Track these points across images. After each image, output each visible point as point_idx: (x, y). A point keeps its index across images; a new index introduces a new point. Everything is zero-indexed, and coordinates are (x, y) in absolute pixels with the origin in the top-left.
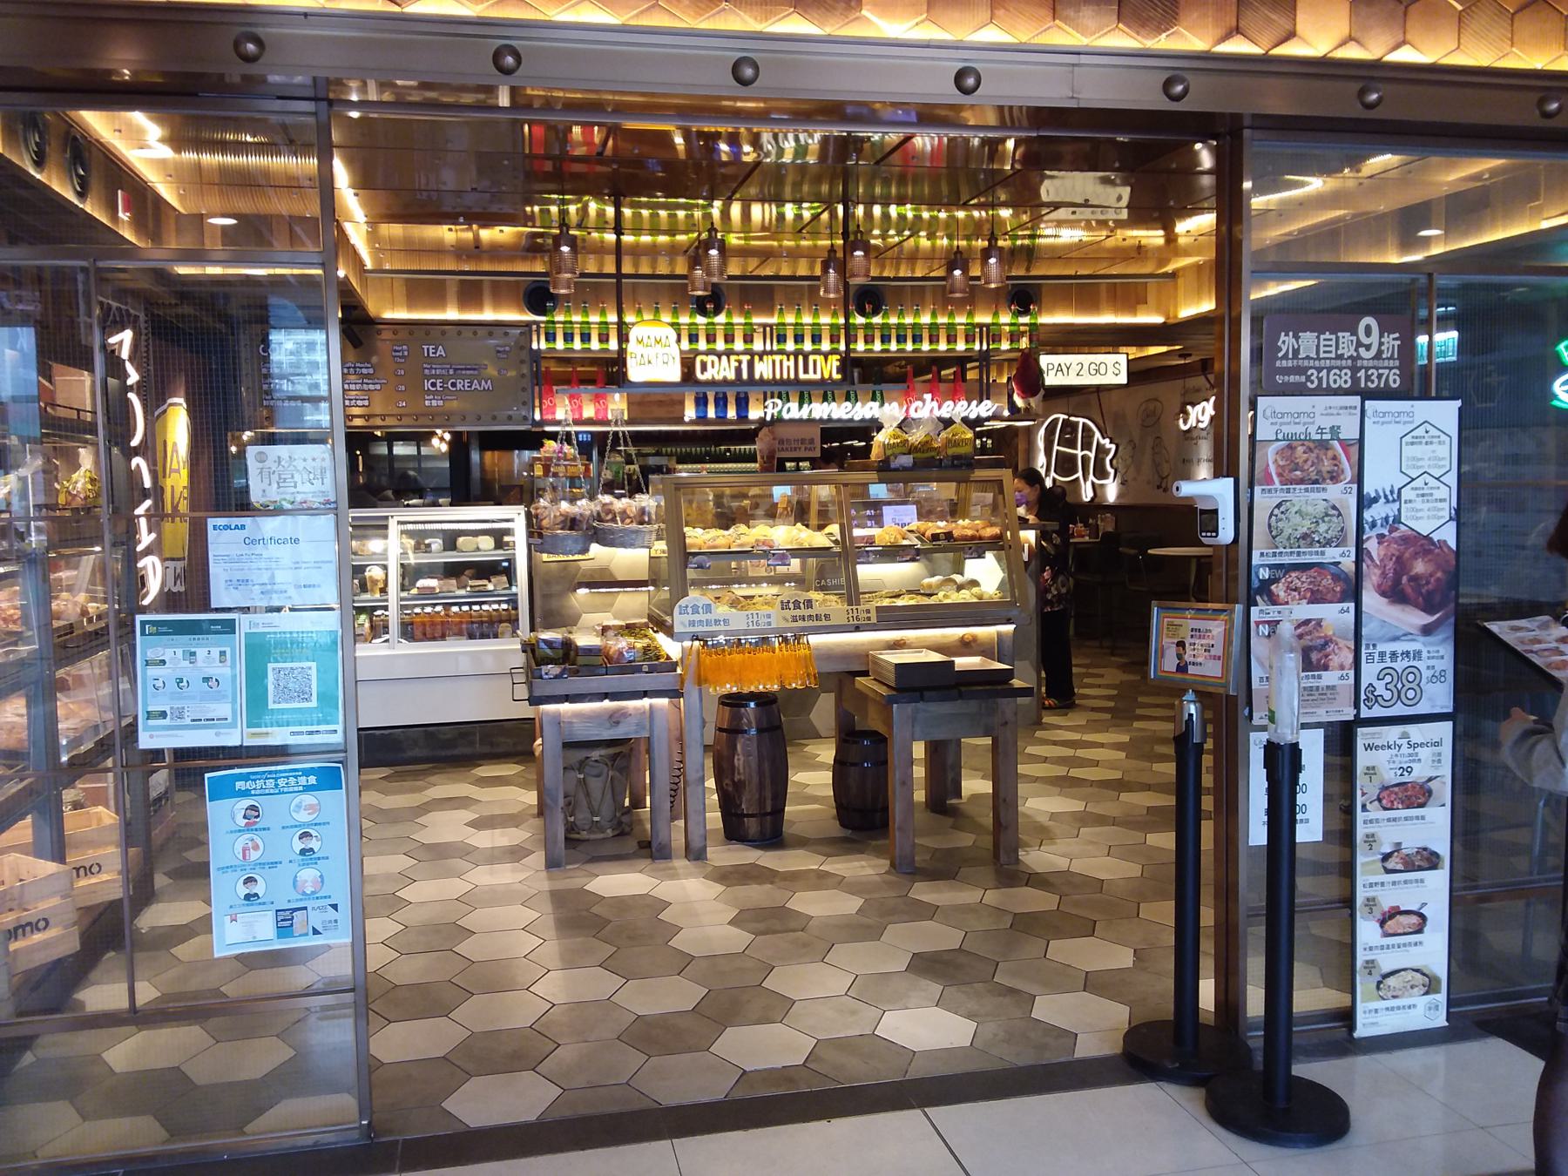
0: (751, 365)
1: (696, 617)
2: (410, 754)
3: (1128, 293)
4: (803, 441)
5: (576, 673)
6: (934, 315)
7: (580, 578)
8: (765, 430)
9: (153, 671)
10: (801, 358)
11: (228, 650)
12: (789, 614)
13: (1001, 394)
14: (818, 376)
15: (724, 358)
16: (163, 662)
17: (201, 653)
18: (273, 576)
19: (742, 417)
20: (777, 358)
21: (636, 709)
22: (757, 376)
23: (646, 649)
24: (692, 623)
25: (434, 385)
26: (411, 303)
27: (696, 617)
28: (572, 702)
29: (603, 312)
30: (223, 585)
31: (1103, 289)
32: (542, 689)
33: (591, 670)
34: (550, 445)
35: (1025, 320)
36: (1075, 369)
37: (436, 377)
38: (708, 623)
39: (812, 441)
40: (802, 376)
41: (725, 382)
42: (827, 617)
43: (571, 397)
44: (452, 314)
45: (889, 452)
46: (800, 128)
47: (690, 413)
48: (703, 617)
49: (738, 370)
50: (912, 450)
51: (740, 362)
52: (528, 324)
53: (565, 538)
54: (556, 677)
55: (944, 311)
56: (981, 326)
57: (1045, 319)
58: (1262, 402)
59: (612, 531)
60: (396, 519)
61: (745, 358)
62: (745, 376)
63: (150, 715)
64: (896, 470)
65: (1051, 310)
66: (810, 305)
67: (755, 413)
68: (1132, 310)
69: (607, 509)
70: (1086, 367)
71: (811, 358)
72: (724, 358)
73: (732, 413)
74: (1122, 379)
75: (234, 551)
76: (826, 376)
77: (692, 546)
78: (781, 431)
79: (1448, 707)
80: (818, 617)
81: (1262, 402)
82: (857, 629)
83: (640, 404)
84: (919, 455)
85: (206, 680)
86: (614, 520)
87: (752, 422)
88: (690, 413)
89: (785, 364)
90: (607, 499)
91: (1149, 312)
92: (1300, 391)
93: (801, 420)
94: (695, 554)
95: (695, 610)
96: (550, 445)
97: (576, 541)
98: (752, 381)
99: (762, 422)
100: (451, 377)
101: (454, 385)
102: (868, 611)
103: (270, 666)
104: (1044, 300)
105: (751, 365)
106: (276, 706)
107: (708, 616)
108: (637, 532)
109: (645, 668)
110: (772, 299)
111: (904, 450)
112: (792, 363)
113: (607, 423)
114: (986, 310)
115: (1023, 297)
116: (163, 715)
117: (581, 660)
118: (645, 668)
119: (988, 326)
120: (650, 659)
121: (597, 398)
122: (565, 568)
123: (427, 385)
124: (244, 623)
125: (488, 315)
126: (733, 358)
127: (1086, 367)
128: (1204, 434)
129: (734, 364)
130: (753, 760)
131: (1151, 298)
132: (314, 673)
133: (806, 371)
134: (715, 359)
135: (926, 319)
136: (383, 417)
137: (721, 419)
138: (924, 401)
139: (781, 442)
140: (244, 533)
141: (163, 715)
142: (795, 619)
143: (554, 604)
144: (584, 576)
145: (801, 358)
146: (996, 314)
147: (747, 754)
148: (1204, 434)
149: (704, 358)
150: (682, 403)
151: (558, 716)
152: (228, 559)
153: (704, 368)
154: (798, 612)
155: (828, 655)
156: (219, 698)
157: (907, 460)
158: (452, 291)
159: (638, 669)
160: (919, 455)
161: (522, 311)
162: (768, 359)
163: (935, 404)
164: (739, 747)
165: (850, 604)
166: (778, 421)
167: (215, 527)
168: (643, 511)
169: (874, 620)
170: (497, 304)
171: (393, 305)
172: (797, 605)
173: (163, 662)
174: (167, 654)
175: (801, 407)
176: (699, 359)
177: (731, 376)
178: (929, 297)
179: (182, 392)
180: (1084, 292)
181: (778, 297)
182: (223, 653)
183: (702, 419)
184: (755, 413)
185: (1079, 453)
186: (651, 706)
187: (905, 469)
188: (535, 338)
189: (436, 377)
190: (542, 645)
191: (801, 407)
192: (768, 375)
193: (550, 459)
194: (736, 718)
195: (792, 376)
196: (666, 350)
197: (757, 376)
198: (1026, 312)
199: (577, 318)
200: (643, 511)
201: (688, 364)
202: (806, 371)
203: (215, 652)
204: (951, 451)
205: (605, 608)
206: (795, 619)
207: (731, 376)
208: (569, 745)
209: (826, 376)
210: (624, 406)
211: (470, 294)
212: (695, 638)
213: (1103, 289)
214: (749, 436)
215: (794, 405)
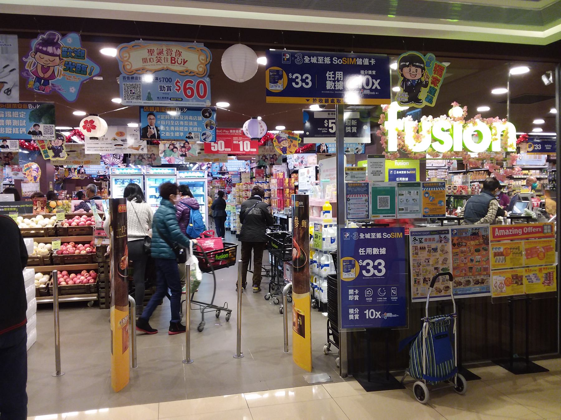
9: (401, 197)
16: (403, 195)
17: (412, 192)
58: (556, 290)
63: (400, 210)
79: (427, 161)
81: (556, 290)
85: (413, 200)
92: (72, 235)
116: (403, 209)
130: (111, 249)
132: (44, 156)
141: (403, 209)
156: (416, 205)
173: (403, 195)
174: (404, 192)
179: (449, 75)
182: (417, 192)
185: (427, 300)
199: (33, 279)
203: (416, 192)
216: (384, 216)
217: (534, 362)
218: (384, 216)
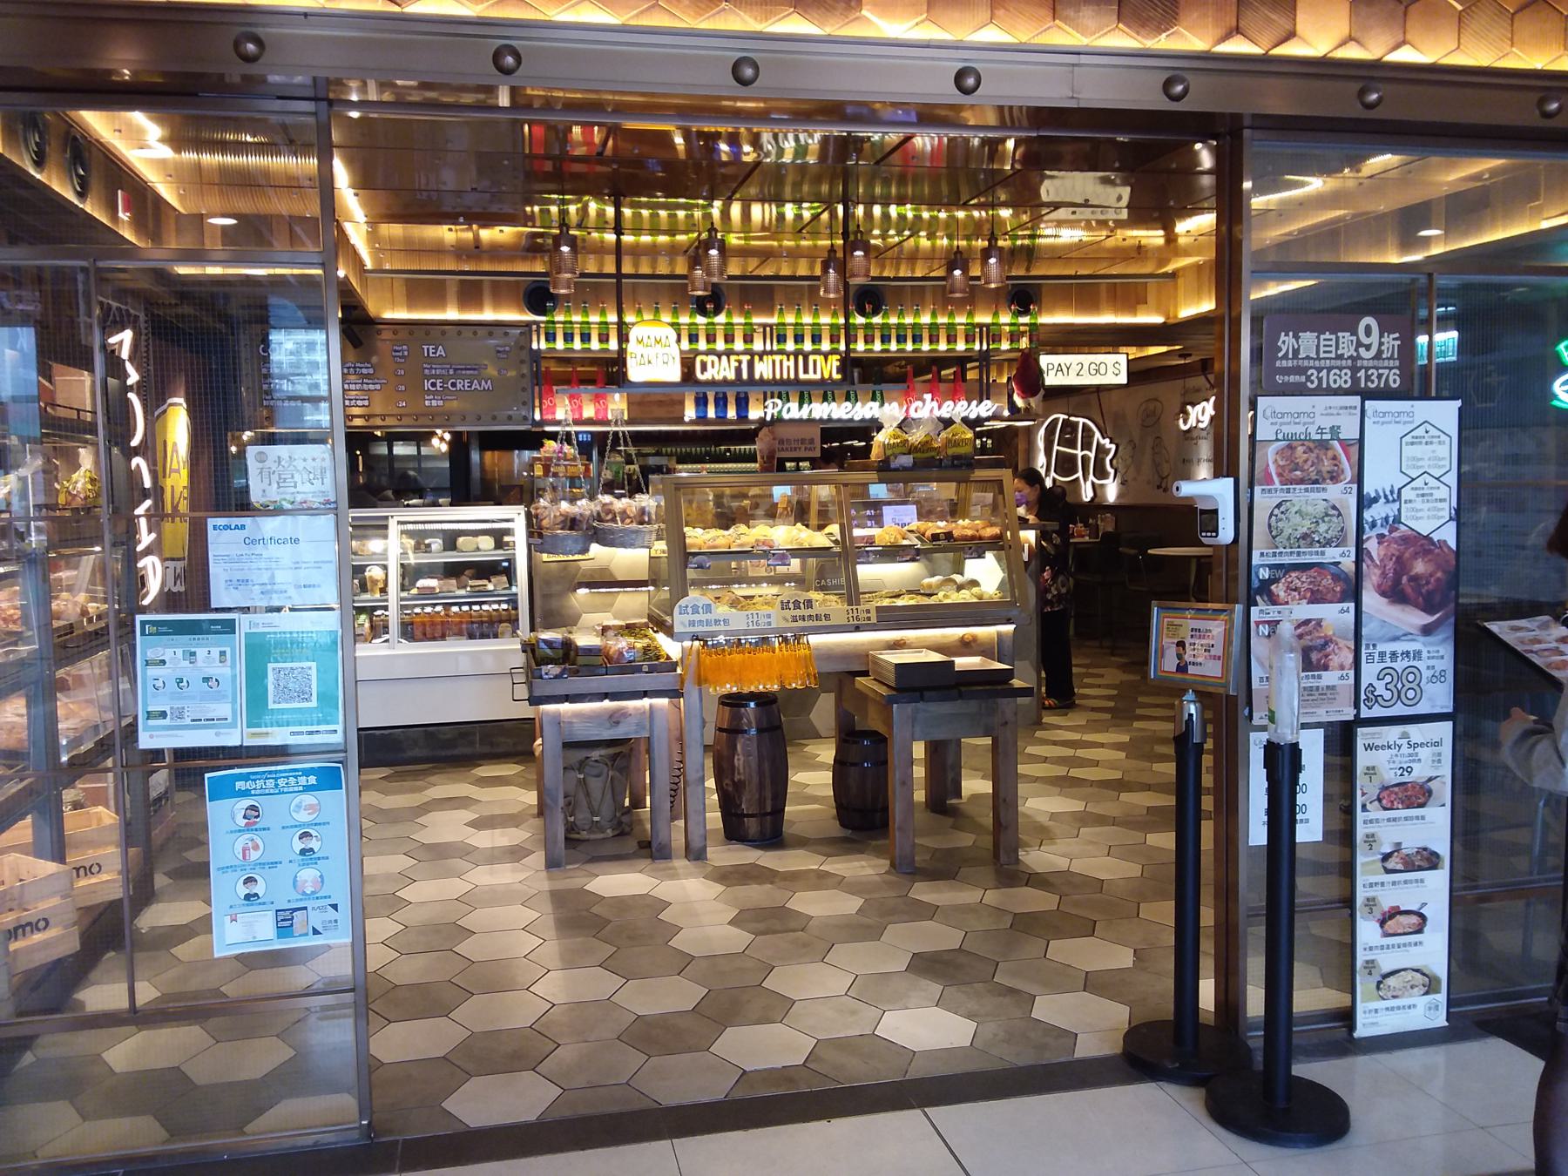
0: (751, 365)
1: (696, 617)
2: (410, 754)
3: (1128, 293)
4: (803, 441)
5: (576, 673)
6: (934, 315)
7: (580, 578)
8: (765, 430)
9: (153, 671)
10: (801, 358)
11: (228, 650)
12: (789, 614)
13: (1001, 394)
14: (818, 376)
15: (724, 358)
16: (163, 662)
17: (201, 653)
18: (273, 576)
19: (742, 417)
20: (777, 358)
21: (636, 709)
22: (757, 376)
23: (646, 649)
24: (692, 623)
25: (434, 385)
26: (411, 303)
27: (696, 617)
28: (572, 702)
29: (603, 312)
30: (223, 585)
31: (1103, 289)
32: (542, 689)
33: (591, 670)
34: (550, 445)
35: (1025, 320)
36: (1075, 369)
37: (436, 377)
38: (708, 623)
39: (812, 441)
40: (802, 376)
41: (725, 382)
42: (827, 617)
43: (571, 397)
44: (452, 314)
45: (889, 452)
46: (800, 128)
47: (690, 413)
48: (703, 617)
49: (738, 370)
50: (912, 450)
51: (740, 362)
52: (528, 324)
53: (565, 538)
54: (556, 677)
55: (944, 311)
56: (981, 326)
57: (1045, 319)
58: (1262, 402)
59: (612, 531)
60: (396, 519)
61: (745, 358)
62: (745, 376)
63: (150, 715)
64: (896, 470)
65: (1051, 310)
66: (810, 305)
67: (755, 413)
68: (1132, 310)
69: (607, 509)
70: (1086, 367)
71: (811, 358)
72: (724, 358)
73: (732, 413)
74: (1122, 379)
75: (234, 551)
76: (826, 376)
77: (692, 546)
78: (781, 431)
80: (818, 617)
81: (1262, 402)
82: (857, 629)
83: (640, 404)
84: (919, 455)
85: (206, 680)
86: (614, 520)
87: (752, 422)
88: (690, 413)
89: (785, 364)
90: (607, 499)
91: (1149, 312)
93: (801, 420)
94: (695, 554)
95: (695, 610)
96: (550, 445)
97: (576, 541)
98: (752, 381)
99: (762, 422)
100: (451, 377)
101: (454, 385)
102: (868, 611)
103: (270, 666)
104: (1044, 300)
105: (751, 365)
106: (276, 706)
107: (708, 616)
108: (637, 532)
109: (645, 668)
110: (772, 299)
111: (904, 450)
112: (792, 363)
113: (607, 423)
114: (986, 310)
115: (1023, 297)
116: (163, 715)
117: (581, 660)
118: (645, 668)
119: (988, 326)
120: (650, 659)
121: (597, 398)
122: (565, 568)
123: (427, 385)
124: (244, 623)
125: (488, 315)
126: (733, 358)
127: (1086, 367)
128: (1204, 434)
129: (734, 364)
130: (753, 760)
131: (1151, 298)
132: (314, 673)
133: (806, 371)
134: (715, 359)
135: (926, 319)
136: (383, 417)
137: (721, 419)
138: (924, 401)
139: (781, 442)
140: (244, 533)
141: (163, 715)
142: (795, 619)
143: (554, 604)
144: (584, 576)
145: (801, 358)
146: (996, 314)
147: (747, 754)
148: (1204, 434)
149: (704, 358)
150: (682, 403)
151: (558, 716)
152: (228, 559)
153: (704, 368)
154: (798, 612)
155: (828, 655)
156: (219, 698)
157: (907, 460)
158: (452, 291)
159: (638, 669)
160: (919, 455)
161: (522, 311)
162: (768, 359)
163: (935, 404)
164: (739, 747)
165: (850, 604)
166: (778, 421)
167: (215, 527)
168: (643, 511)
169: (874, 620)
170: (497, 304)
171: (393, 305)
172: (797, 605)
173: (163, 662)
174: (167, 654)
175: (801, 407)
176: (699, 359)
177: (731, 376)
178: (929, 297)
179: (182, 392)
180: (1084, 292)
181: (778, 297)
182: (223, 653)
183: (702, 419)
184: (755, 413)
186: (651, 706)
187: (905, 469)
188: (535, 338)
189: (436, 377)
190: (542, 645)
191: (801, 407)
192: (768, 375)
193: (550, 459)
194: (736, 718)
195: (792, 376)
196: (666, 350)
197: (757, 376)
198: (1026, 312)
200: (643, 511)
201: (688, 364)
202: (806, 371)
203: (215, 652)
204: (951, 451)
205: (605, 608)
206: (795, 619)
207: (731, 376)
208: (569, 745)
209: (826, 376)
210: (624, 406)
211: (470, 294)
212: (695, 638)
213: (1103, 289)
214: (749, 436)
215: (794, 405)
216: (293, 733)
217: (1494, 627)
218: (293, 733)
